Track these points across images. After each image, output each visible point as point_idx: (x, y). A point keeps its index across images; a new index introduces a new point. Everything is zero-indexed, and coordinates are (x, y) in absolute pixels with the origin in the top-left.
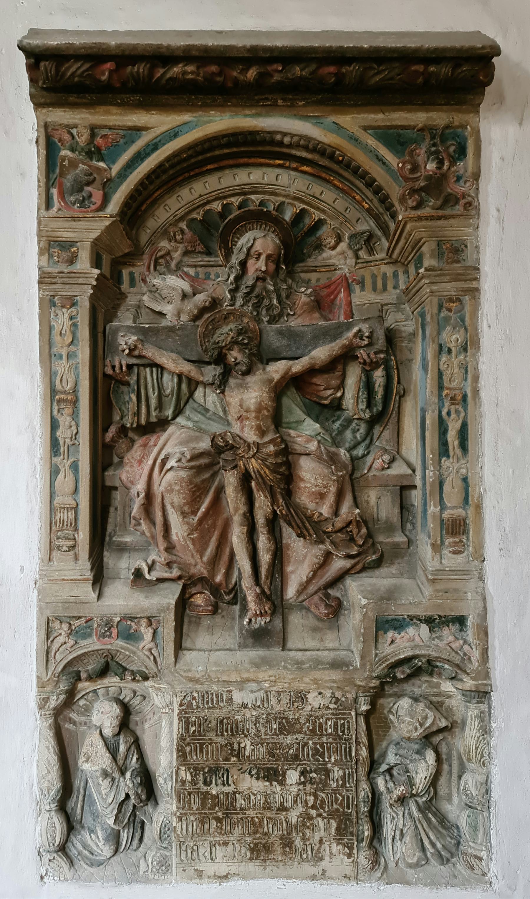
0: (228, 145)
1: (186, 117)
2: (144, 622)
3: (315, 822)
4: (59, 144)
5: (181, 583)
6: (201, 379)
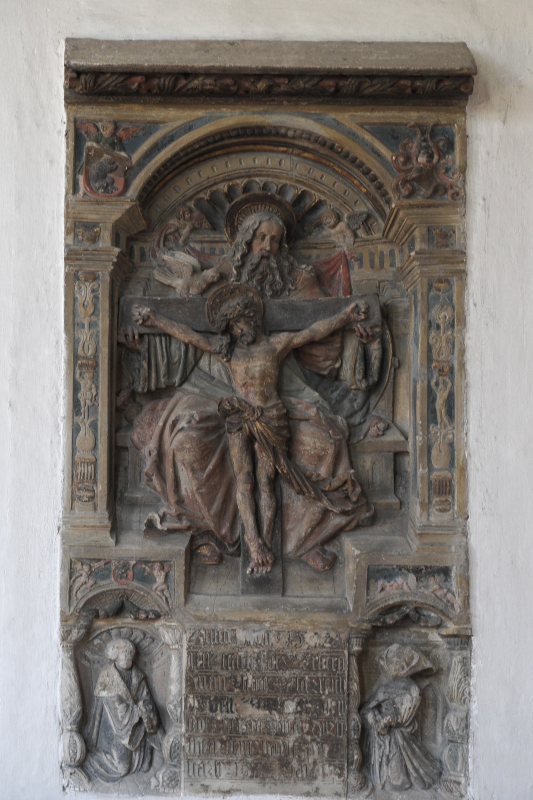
0: (238, 136)
1: (200, 113)
2: (157, 566)
3: (310, 746)
4: (86, 136)
5: (189, 534)
6: (209, 348)
